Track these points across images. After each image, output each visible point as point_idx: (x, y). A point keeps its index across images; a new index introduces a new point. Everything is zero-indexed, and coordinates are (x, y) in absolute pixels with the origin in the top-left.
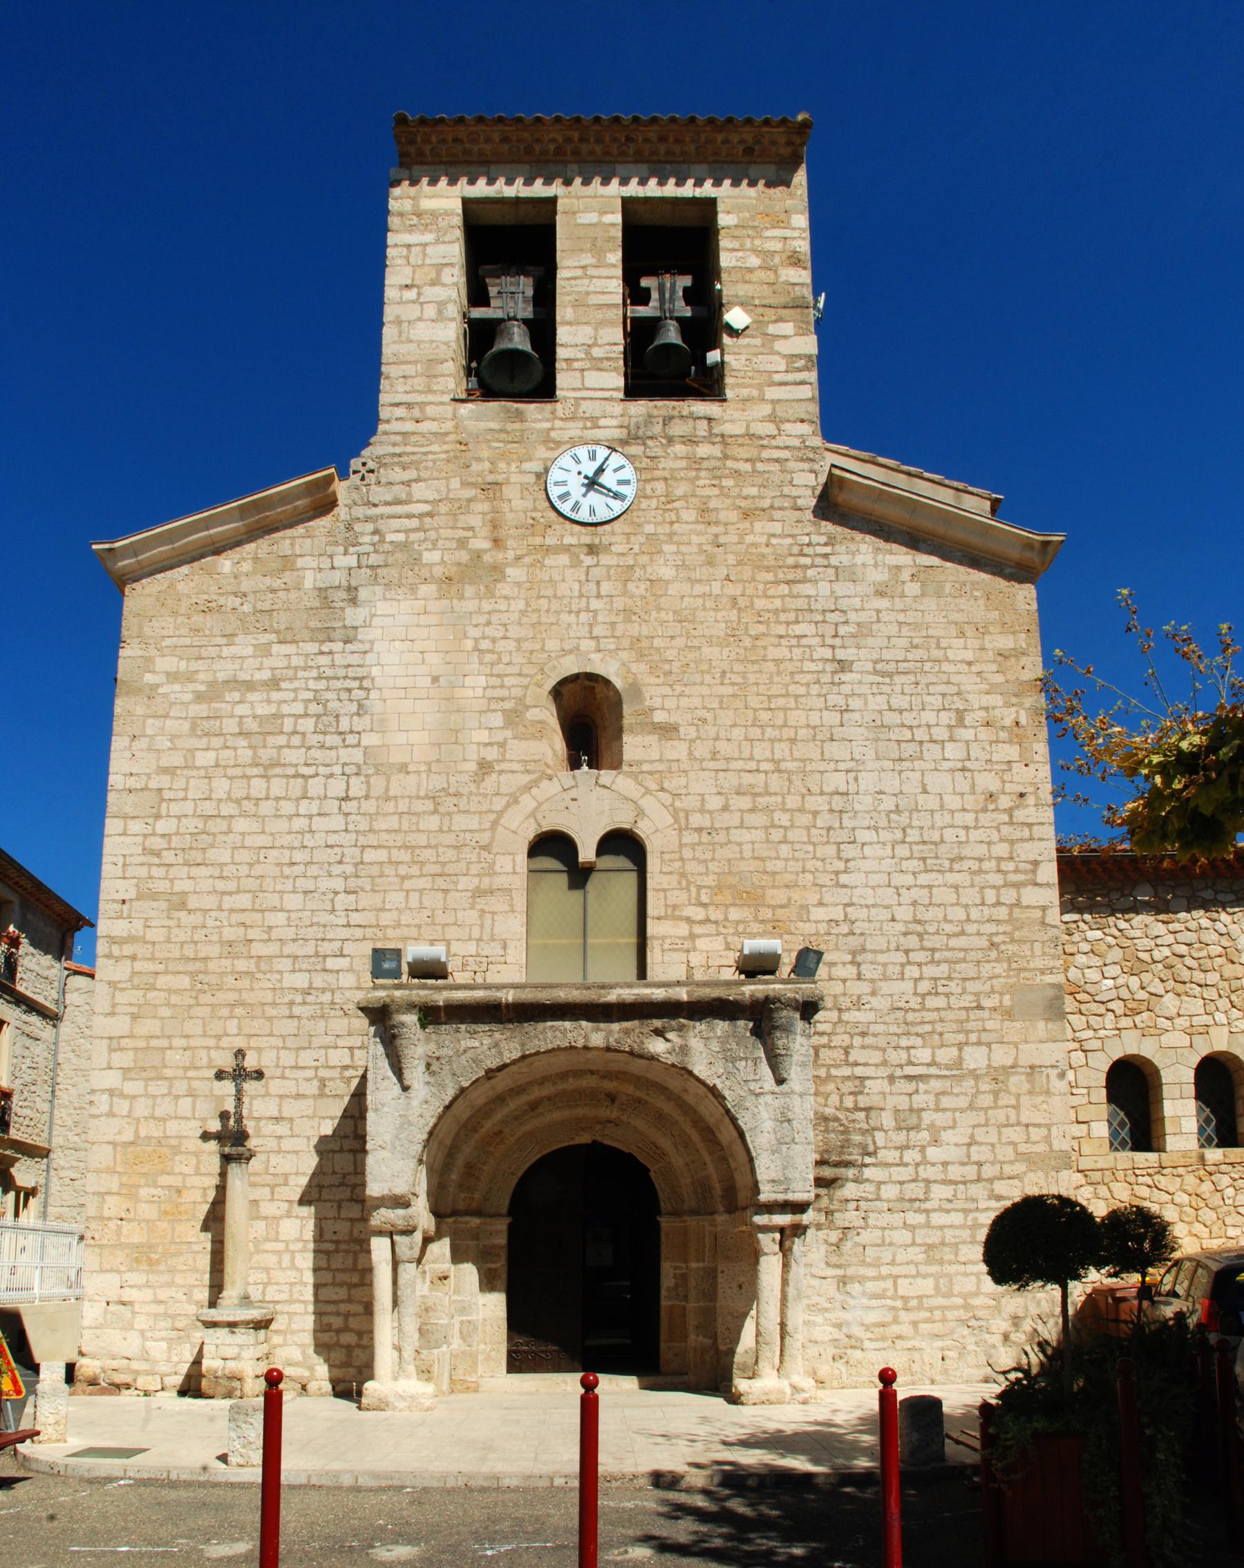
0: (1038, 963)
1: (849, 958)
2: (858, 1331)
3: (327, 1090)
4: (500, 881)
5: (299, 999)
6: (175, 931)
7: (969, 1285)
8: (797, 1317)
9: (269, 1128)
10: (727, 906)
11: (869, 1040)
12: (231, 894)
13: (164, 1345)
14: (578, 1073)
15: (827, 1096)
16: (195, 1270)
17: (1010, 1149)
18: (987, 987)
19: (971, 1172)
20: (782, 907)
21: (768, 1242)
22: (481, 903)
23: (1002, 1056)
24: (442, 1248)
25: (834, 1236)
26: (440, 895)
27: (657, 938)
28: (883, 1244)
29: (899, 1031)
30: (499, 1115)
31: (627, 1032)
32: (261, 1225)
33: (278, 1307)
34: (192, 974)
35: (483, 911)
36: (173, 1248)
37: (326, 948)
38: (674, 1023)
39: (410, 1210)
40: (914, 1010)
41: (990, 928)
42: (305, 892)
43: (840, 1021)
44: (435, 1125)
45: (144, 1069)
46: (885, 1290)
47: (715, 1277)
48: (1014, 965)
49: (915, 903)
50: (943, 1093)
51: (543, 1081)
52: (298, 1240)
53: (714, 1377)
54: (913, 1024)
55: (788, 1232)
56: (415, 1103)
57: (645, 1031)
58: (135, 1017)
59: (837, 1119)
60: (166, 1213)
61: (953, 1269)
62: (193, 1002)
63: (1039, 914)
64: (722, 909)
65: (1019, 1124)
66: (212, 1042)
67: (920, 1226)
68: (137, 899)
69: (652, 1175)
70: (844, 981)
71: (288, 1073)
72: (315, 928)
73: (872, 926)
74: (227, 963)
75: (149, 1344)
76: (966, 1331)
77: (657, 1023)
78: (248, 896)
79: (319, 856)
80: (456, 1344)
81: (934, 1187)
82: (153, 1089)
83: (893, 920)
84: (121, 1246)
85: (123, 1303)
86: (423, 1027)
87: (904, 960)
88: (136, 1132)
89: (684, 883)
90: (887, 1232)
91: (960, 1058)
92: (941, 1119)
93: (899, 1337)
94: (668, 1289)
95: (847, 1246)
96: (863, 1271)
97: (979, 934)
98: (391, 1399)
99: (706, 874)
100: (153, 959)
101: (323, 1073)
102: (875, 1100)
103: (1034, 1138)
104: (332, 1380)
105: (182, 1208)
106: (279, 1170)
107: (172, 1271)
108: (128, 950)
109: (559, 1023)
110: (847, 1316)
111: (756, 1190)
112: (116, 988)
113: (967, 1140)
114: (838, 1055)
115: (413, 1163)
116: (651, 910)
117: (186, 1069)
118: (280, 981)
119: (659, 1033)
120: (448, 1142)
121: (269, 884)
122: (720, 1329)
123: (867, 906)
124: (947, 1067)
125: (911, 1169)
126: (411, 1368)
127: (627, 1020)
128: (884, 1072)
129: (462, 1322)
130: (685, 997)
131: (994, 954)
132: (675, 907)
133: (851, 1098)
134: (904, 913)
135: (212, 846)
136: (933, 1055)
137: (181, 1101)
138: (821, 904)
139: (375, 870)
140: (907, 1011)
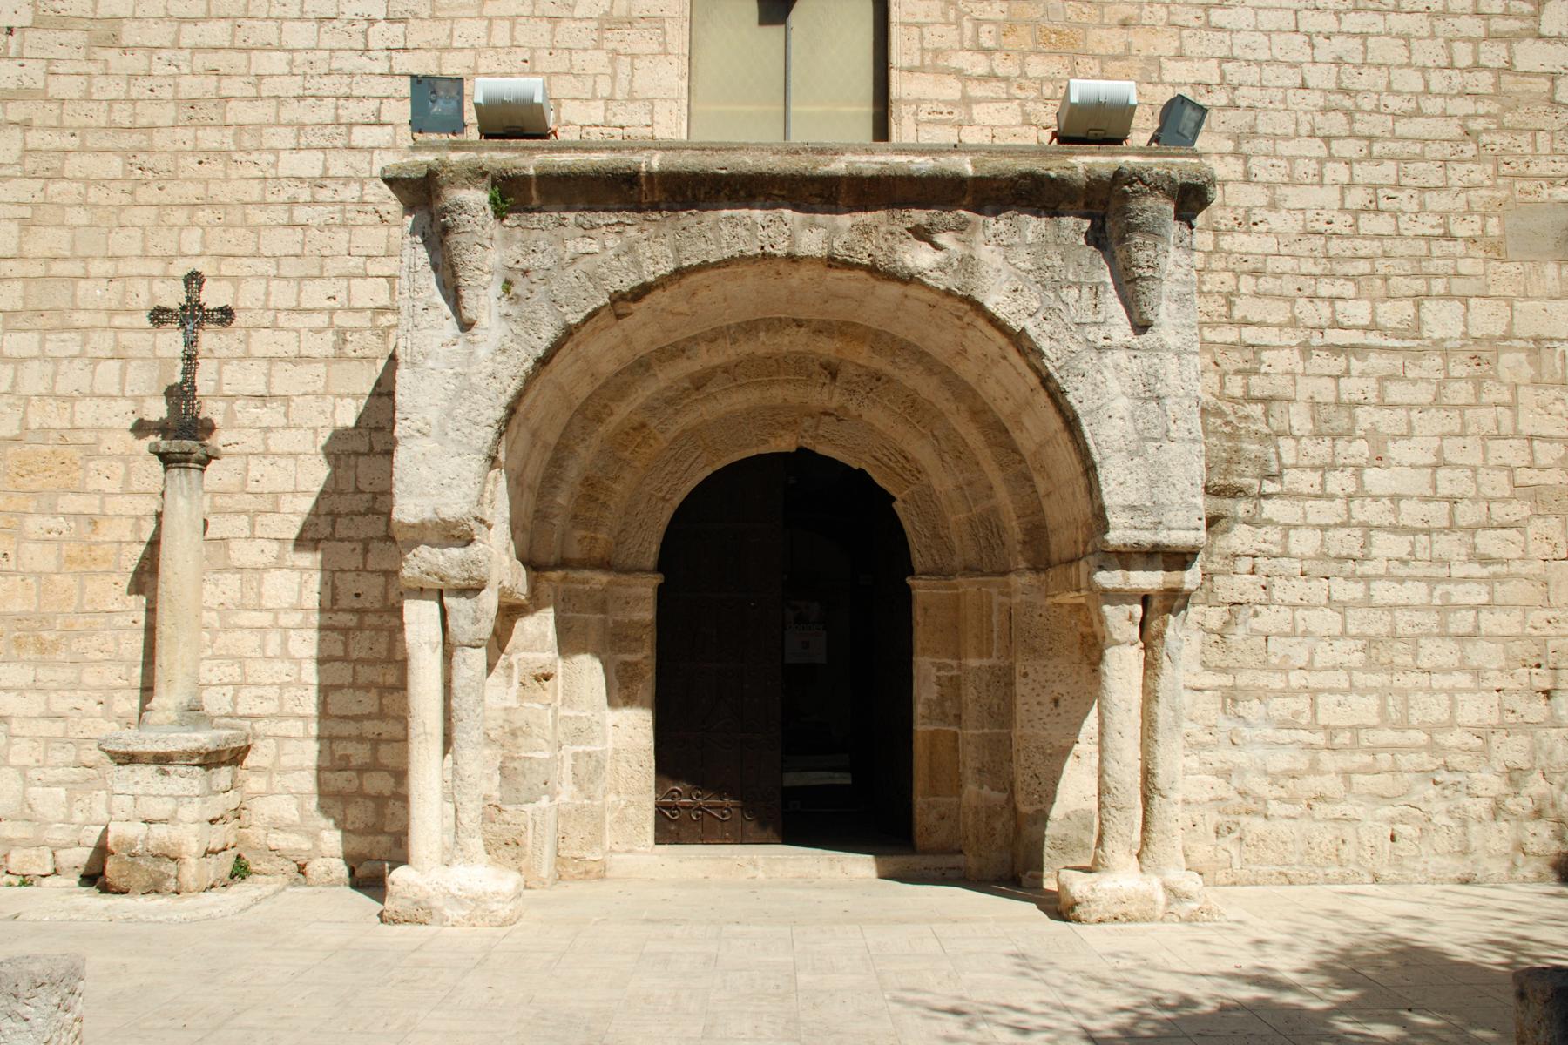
0: (1543, 167)
1: (1229, 146)
2: (1258, 785)
3: (349, 349)
5: (305, 195)
8: (1173, 761)
9: (249, 413)
10: (1024, 54)
11: (1266, 284)
13: (61, 792)
14: (775, 325)
16: (118, 660)
17: (1502, 477)
18: (1460, 204)
19: (1438, 513)
20: (1116, 58)
21: (1121, 621)
22: (613, 40)
23: (1487, 320)
24: (539, 627)
25: (1215, 617)
26: (545, 26)
27: (908, 103)
28: (1293, 633)
29: (1317, 270)
30: (644, 393)
32: (231, 581)
33: (259, 726)
34: (128, 154)
35: (616, 52)
36: (81, 622)
37: (352, 111)
38: (949, 217)
39: (472, 550)
41: (1464, 106)
42: (321, 20)
43: (1217, 249)
44: (520, 396)
46: (1296, 714)
47: (1010, 684)
48: (1504, 169)
49: (1338, 61)
50: (1391, 377)
51: (714, 336)
52: (294, 608)
54: (1339, 259)
55: (1156, 603)
56: (482, 352)
58: (26, 224)
60: (70, 560)
61: (1409, 680)
62: (126, 199)
63: (1544, 85)
64: (1016, 57)
65: (1516, 435)
66: (156, 268)
68: (33, 27)
69: (898, 506)
71: (283, 319)
72: (335, 78)
73: (1267, 94)
74: (188, 134)
75: (35, 792)
76: (1431, 791)
77: (920, 216)
80: (567, 793)
81: (1379, 538)
82: (53, 348)
83: (1304, 87)
86: (500, 215)
87: (1323, 153)
88: (24, 420)
89: (952, 15)
90: (1300, 613)
91: (1418, 318)
92: (1387, 421)
93: (1320, 798)
94: (928, 703)
95: (1238, 635)
97: (1445, 115)
98: (436, 903)
100: (60, 128)
101: (341, 319)
102: (1281, 386)
103: (1542, 460)
104: (348, 858)
105: (99, 552)
106: (265, 486)
109: (744, 212)
110: (1239, 757)
111: (1099, 520)
113: (1431, 459)
115: (477, 463)
116: (897, 57)
117: (112, 312)
118: (275, 165)
119: (922, 234)
120: (552, 437)
122: (1021, 777)
123: (1258, 63)
125: (1339, 505)
126: (476, 844)
127: (866, 209)
129: (576, 755)
130: (969, 170)
131: (1470, 150)
132: (937, 53)
134: (1321, 77)
136: (1373, 312)
137: (101, 367)
138: (1180, 56)
140: (1329, 237)
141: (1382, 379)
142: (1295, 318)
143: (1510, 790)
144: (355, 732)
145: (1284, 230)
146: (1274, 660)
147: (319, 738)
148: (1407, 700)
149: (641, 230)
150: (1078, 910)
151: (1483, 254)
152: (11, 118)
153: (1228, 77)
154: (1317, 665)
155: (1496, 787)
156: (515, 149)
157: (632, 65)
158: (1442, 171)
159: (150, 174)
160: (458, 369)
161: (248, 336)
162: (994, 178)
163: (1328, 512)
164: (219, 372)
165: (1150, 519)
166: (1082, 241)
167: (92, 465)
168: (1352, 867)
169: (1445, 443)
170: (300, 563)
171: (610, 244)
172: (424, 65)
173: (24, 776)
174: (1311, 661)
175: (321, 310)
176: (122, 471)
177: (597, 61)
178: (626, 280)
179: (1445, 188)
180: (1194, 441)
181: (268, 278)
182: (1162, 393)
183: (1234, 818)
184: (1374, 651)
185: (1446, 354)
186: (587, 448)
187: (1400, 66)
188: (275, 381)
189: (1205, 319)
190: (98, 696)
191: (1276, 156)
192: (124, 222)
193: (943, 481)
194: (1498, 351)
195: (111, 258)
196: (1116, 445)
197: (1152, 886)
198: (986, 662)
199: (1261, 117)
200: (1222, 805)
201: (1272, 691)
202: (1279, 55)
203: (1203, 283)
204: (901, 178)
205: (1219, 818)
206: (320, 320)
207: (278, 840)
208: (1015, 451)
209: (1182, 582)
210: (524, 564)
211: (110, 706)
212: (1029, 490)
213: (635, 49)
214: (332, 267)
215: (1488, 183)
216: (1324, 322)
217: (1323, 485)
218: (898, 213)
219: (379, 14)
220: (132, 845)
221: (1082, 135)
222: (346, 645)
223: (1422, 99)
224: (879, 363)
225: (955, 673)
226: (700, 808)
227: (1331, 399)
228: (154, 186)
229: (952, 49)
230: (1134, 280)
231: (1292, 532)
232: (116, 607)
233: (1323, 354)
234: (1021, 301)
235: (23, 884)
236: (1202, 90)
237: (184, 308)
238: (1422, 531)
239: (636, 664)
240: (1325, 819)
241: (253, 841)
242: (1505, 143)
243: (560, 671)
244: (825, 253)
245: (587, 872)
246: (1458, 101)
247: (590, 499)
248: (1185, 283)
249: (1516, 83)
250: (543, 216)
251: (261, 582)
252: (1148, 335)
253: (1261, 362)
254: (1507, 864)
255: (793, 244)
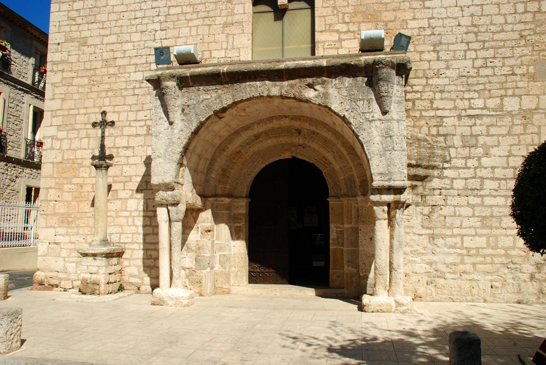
3: (150, 132)
4: (237, 18)
6: (82, 56)
7: (509, 242)
8: (399, 259)
9: (123, 152)
10: (360, 23)
11: (445, 95)
12: (107, 36)
13: (74, 265)
14: (279, 118)
15: (421, 128)
18: (519, 62)
21: (381, 212)
22: (227, 30)
23: (528, 103)
24: (206, 216)
25: (426, 210)
26: (207, 28)
28: (454, 216)
29: (464, 89)
31: (292, 86)
32: (119, 203)
33: (127, 246)
34: (89, 77)
35: (228, 34)
36: (79, 215)
39: (174, 192)
40: (472, 77)
41: (521, 27)
42: (142, 32)
43: (427, 84)
45: (67, 125)
47: (357, 233)
49: (472, 15)
50: (491, 125)
51: (259, 122)
53: (353, 291)
54: (472, 85)
55: (392, 206)
56: (176, 131)
57: (303, 85)
58: (63, 100)
59: (425, 140)
60: (76, 197)
61: (499, 231)
62: (89, 90)
64: (357, 24)
67: (477, 205)
68: (65, 42)
70: (429, 61)
72: (146, 49)
73: (445, 29)
76: (506, 271)
77: (309, 80)
78: (115, 36)
79: (148, 13)
81: (487, 182)
82: (71, 135)
83: (459, 25)
84: (56, 214)
85: (56, 244)
86: (181, 89)
87: (466, 48)
88: (63, 157)
89: (335, 12)
90: (457, 208)
92: (490, 141)
93: (465, 272)
94: (333, 239)
95: (435, 216)
96: (444, 231)
97: (513, 31)
98: (166, 299)
99: (348, 6)
100: (71, 71)
102: (450, 130)
105: (83, 195)
107: (78, 227)
108: (60, 67)
109: (254, 83)
110: (435, 258)
112: (55, 86)
114: (427, 104)
116: (317, 28)
118: (129, 77)
119: (311, 86)
120: (209, 157)
121: (125, 29)
123: (442, 19)
124: (494, 110)
125: (472, 171)
128: (455, 113)
129: (220, 255)
131: (523, 42)
132: (330, 25)
133: (435, 129)
135: (99, 13)
136: (485, 103)
138: (414, 19)
139: (175, 18)
140: (468, 77)
141: (488, 126)
142: (456, 106)
143: (537, 271)
144: (153, 248)
145: (452, 76)
146: (448, 225)
147: (143, 249)
148: (497, 238)
149: (223, 91)
150: (365, 308)
151: (527, 80)
152: (59, 69)
153: (431, 24)
154: (463, 226)
155: (531, 270)
156: (185, 68)
157: (233, 38)
158: (511, 51)
159: (95, 83)
160: (169, 137)
161: (122, 129)
162: (333, 66)
163: (468, 173)
164: (115, 140)
165: (388, 177)
166: (364, 85)
167: (81, 169)
168: (476, 296)
169: (512, 148)
170: (137, 197)
171: (213, 96)
172: (158, 45)
173: (64, 260)
174: (461, 225)
175: (142, 120)
176: (89, 171)
177: (222, 37)
178: (218, 107)
179: (513, 57)
180: (403, 150)
181: (128, 111)
182: (392, 135)
183: (433, 279)
184: (485, 222)
185: (512, 116)
186: (221, 159)
187: (496, 15)
188: (130, 142)
189: (423, 108)
190: (83, 237)
191: (449, 51)
192: (89, 97)
193: (337, 167)
194: (533, 114)
195: (85, 108)
196: (376, 153)
197: (391, 301)
198: (350, 226)
199: (443, 37)
200: (429, 274)
201: (447, 235)
202: (449, 15)
203: (422, 96)
204: (302, 68)
205: (427, 279)
206: (142, 123)
207: (132, 280)
208: (357, 155)
209: (400, 198)
210: (200, 195)
211: (86, 240)
212: (362, 169)
213: (234, 32)
214: (146, 107)
215: (529, 54)
216: (466, 107)
217: (466, 164)
218: (303, 80)
219: (158, 29)
220: (87, 280)
221: (367, 49)
222: (150, 221)
223: (504, 26)
224: (313, 128)
225: (342, 229)
226: (262, 272)
227: (469, 134)
228: (96, 86)
229: (335, 23)
230: (381, 97)
231: (454, 181)
232: (88, 211)
233: (466, 118)
234: (343, 106)
235: (64, 291)
236: (422, 30)
237: (101, 122)
238: (503, 179)
239: (240, 227)
240: (466, 280)
241: (125, 280)
242: (537, 38)
243: (215, 229)
244: (279, 94)
245: (224, 292)
246: (518, 25)
247: (224, 175)
248: (400, 97)
249: (542, 16)
250: (193, 88)
251: (127, 203)
252: (387, 115)
253: (443, 122)
254: (536, 297)
255: (269, 92)
